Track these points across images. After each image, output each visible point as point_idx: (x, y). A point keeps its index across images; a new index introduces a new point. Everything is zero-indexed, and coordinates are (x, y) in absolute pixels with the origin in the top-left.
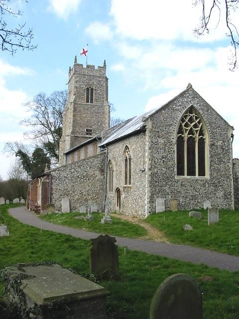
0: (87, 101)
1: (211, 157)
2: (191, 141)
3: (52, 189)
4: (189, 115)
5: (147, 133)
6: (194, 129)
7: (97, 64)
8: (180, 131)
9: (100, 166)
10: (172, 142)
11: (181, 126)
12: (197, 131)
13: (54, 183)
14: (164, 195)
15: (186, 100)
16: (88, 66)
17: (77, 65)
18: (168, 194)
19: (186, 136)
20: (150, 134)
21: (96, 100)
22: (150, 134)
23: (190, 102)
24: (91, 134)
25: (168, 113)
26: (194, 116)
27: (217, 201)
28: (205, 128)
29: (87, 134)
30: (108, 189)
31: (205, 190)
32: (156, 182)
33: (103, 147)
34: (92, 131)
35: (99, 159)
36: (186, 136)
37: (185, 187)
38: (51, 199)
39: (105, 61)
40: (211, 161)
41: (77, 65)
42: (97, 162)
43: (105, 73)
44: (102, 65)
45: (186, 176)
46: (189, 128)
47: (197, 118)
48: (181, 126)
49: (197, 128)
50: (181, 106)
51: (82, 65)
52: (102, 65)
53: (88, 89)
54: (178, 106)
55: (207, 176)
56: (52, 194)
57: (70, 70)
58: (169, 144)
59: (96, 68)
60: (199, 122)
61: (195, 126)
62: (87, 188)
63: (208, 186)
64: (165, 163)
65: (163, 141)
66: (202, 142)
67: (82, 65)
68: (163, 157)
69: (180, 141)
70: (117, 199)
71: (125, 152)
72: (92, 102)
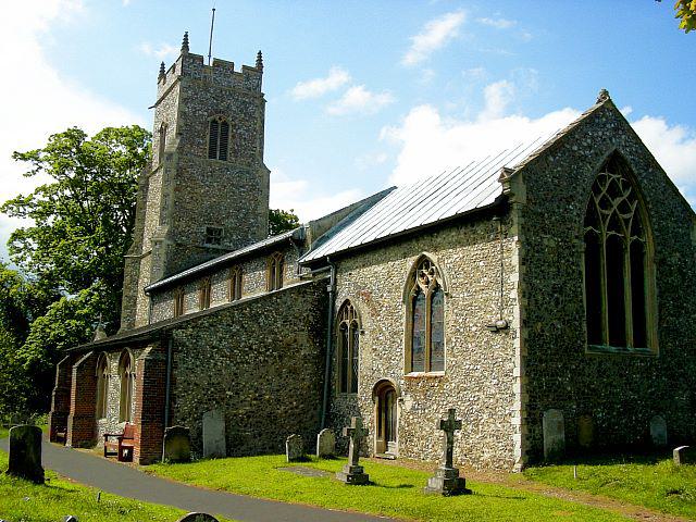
0: (212, 155)
1: (661, 295)
2: (615, 243)
3: (173, 382)
4: (610, 177)
5: (515, 216)
6: (621, 216)
7: (241, 60)
8: (592, 218)
9: (311, 318)
10: (574, 247)
11: (592, 202)
12: (627, 221)
13: (182, 367)
14: (560, 401)
15: (600, 133)
16: (218, 63)
17: (189, 59)
18: (570, 398)
19: (605, 233)
20: (523, 221)
21: (235, 152)
22: (523, 221)
23: (611, 139)
24: (218, 241)
25: (562, 166)
26: (618, 179)
27: (678, 419)
28: (644, 216)
29: (209, 241)
30: (337, 386)
31: (650, 387)
32: (541, 361)
33: (314, 264)
34: (223, 234)
35: (309, 298)
36: (605, 233)
37: (608, 377)
38: (171, 412)
39: (260, 53)
40: (661, 307)
41: (189, 59)
42: (303, 307)
43: (259, 86)
44: (253, 65)
45: (607, 346)
46: (609, 212)
47: (626, 186)
48: (592, 202)
49: (606, 209)
50: (590, 147)
51: (201, 58)
52: (253, 65)
53: (214, 121)
54: (585, 148)
55: (653, 346)
56: (173, 399)
57: (163, 75)
58: (567, 251)
59: (238, 69)
60: (632, 198)
61: (624, 208)
62: (276, 382)
63: (657, 376)
64: (560, 306)
65: (553, 244)
66: (638, 249)
67: (201, 58)
68: (554, 289)
69: (592, 240)
70: (375, 414)
71: (413, 275)
72: (223, 158)
